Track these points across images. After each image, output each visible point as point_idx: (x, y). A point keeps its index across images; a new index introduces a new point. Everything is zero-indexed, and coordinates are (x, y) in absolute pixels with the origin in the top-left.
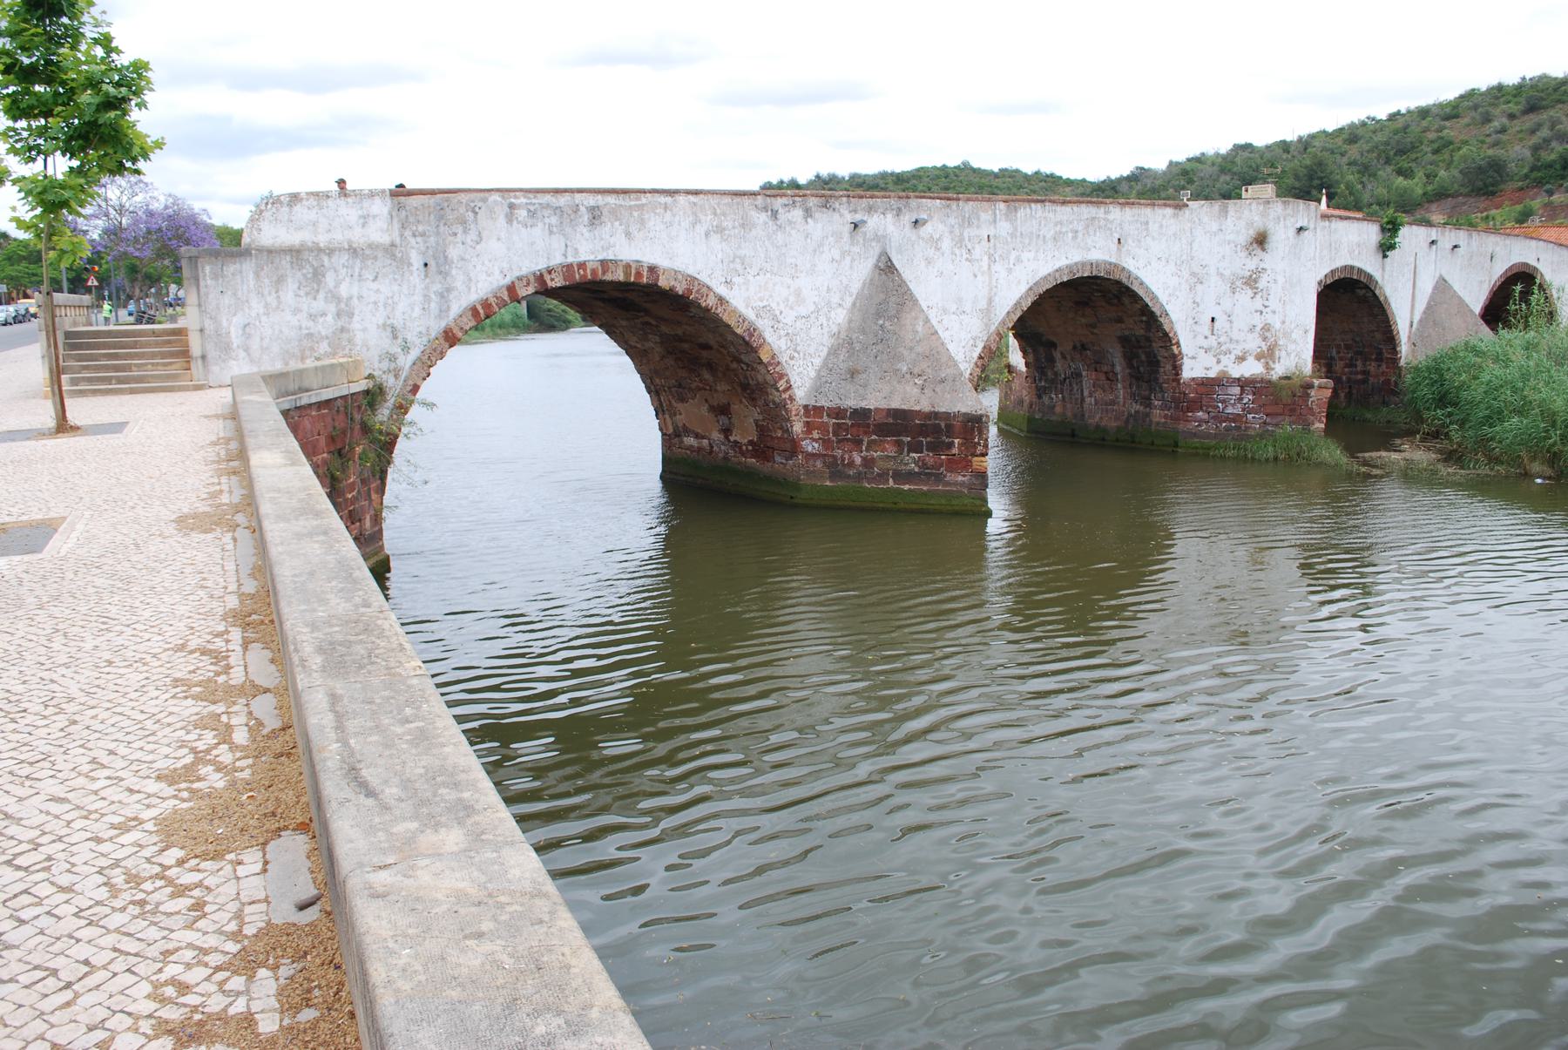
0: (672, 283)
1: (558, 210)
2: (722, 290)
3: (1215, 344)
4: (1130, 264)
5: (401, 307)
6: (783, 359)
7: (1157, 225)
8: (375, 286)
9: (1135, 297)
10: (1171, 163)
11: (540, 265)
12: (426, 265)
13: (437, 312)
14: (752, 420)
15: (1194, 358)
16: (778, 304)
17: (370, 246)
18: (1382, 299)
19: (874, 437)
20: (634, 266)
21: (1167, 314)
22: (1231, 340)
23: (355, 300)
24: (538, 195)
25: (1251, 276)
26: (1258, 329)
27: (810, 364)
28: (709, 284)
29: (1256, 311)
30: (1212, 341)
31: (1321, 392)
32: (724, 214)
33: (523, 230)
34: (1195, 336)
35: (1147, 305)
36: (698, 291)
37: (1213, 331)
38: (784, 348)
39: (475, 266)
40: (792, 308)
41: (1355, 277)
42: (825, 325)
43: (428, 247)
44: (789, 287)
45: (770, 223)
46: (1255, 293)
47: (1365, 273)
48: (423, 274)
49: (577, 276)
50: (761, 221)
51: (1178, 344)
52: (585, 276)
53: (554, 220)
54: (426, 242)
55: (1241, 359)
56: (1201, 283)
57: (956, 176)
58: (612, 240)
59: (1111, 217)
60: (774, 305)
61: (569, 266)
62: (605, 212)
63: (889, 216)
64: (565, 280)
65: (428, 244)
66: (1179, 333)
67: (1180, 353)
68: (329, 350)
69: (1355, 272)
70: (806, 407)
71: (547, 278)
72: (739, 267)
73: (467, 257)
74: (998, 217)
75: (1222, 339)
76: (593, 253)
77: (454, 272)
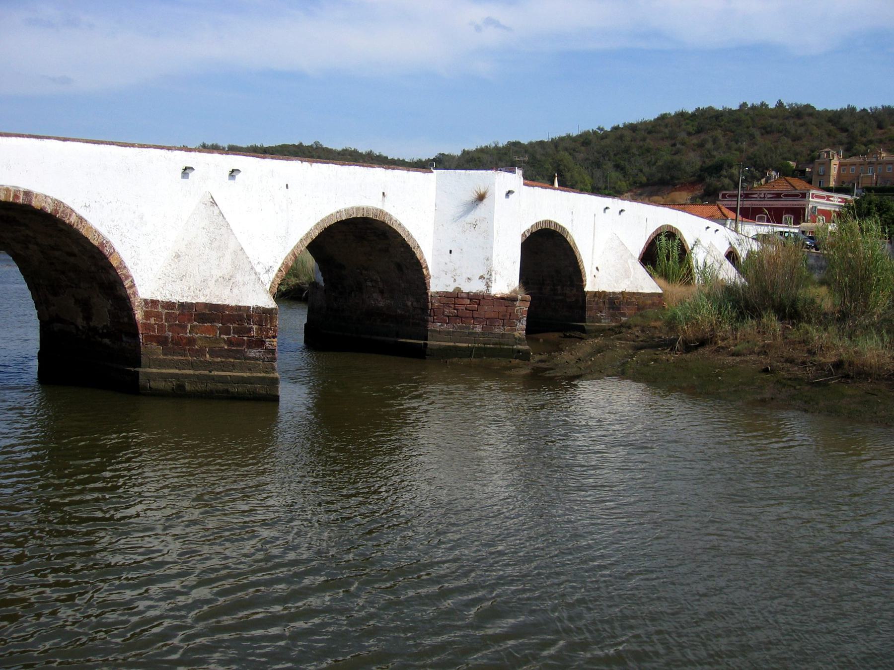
0: (43, 205)
9: (330, 227)
10: (464, 151)
14: (106, 310)
15: (437, 278)
18: (571, 244)
21: (419, 247)
31: (522, 308)
35: (404, 239)
36: (63, 212)
40: (136, 228)
41: (553, 228)
47: (560, 226)
51: (427, 269)
57: (309, 152)
67: (428, 274)
70: (146, 301)
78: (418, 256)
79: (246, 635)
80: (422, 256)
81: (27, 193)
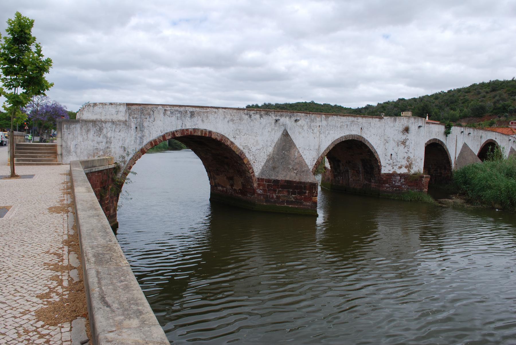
1: (180, 112)
2: (232, 140)
3: (392, 163)
4: (365, 136)
5: (127, 141)
6: (252, 162)
7: (373, 124)
8: (119, 134)
10: (378, 103)
11: (174, 129)
12: (136, 128)
13: (139, 143)
14: (240, 182)
15: (385, 167)
16: (250, 145)
17: (118, 121)
18: (446, 149)
19: (280, 189)
20: (204, 131)
21: (377, 152)
22: (397, 161)
23: (112, 138)
24: (174, 107)
25: (404, 141)
26: (406, 158)
27: (260, 165)
28: (228, 138)
29: (405, 152)
30: (391, 162)
31: (426, 179)
32: (234, 116)
33: (169, 118)
34: (385, 160)
35: (370, 149)
36: (224, 140)
37: (391, 158)
38: (252, 159)
39: (152, 129)
42: (265, 152)
43: (137, 122)
44: (254, 140)
45: (249, 119)
46: (405, 147)
48: (135, 131)
49: (185, 133)
50: (246, 118)
52: (188, 133)
53: (179, 115)
54: (137, 120)
55: (400, 168)
56: (388, 143)
58: (197, 122)
59: (359, 121)
60: (249, 145)
61: (183, 130)
62: (195, 113)
63: (287, 118)
64: (181, 134)
65: (138, 121)
66: (380, 158)
67: (381, 165)
68: (103, 154)
69: (437, 141)
70: (258, 179)
71: (176, 133)
72: (238, 132)
73: (150, 126)
74: (322, 120)
75: (394, 161)
76: (191, 126)
77: (145, 130)
78: (376, 157)
79: (286, 341)
80: (378, 157)
81: (210, 132)
